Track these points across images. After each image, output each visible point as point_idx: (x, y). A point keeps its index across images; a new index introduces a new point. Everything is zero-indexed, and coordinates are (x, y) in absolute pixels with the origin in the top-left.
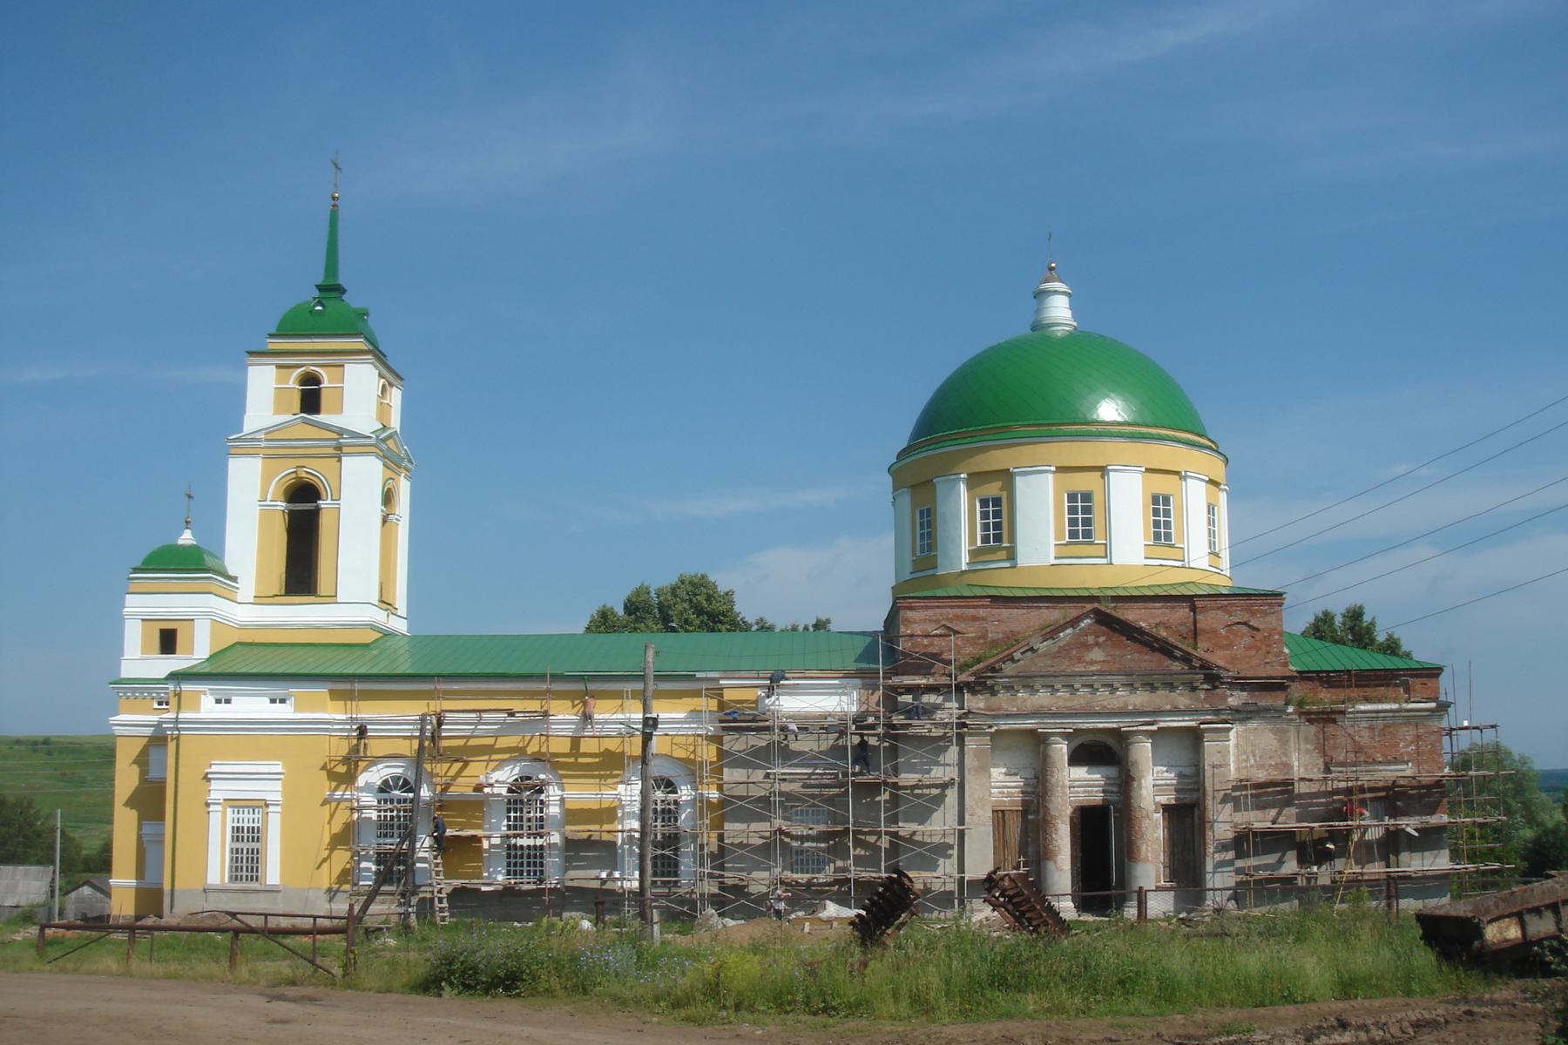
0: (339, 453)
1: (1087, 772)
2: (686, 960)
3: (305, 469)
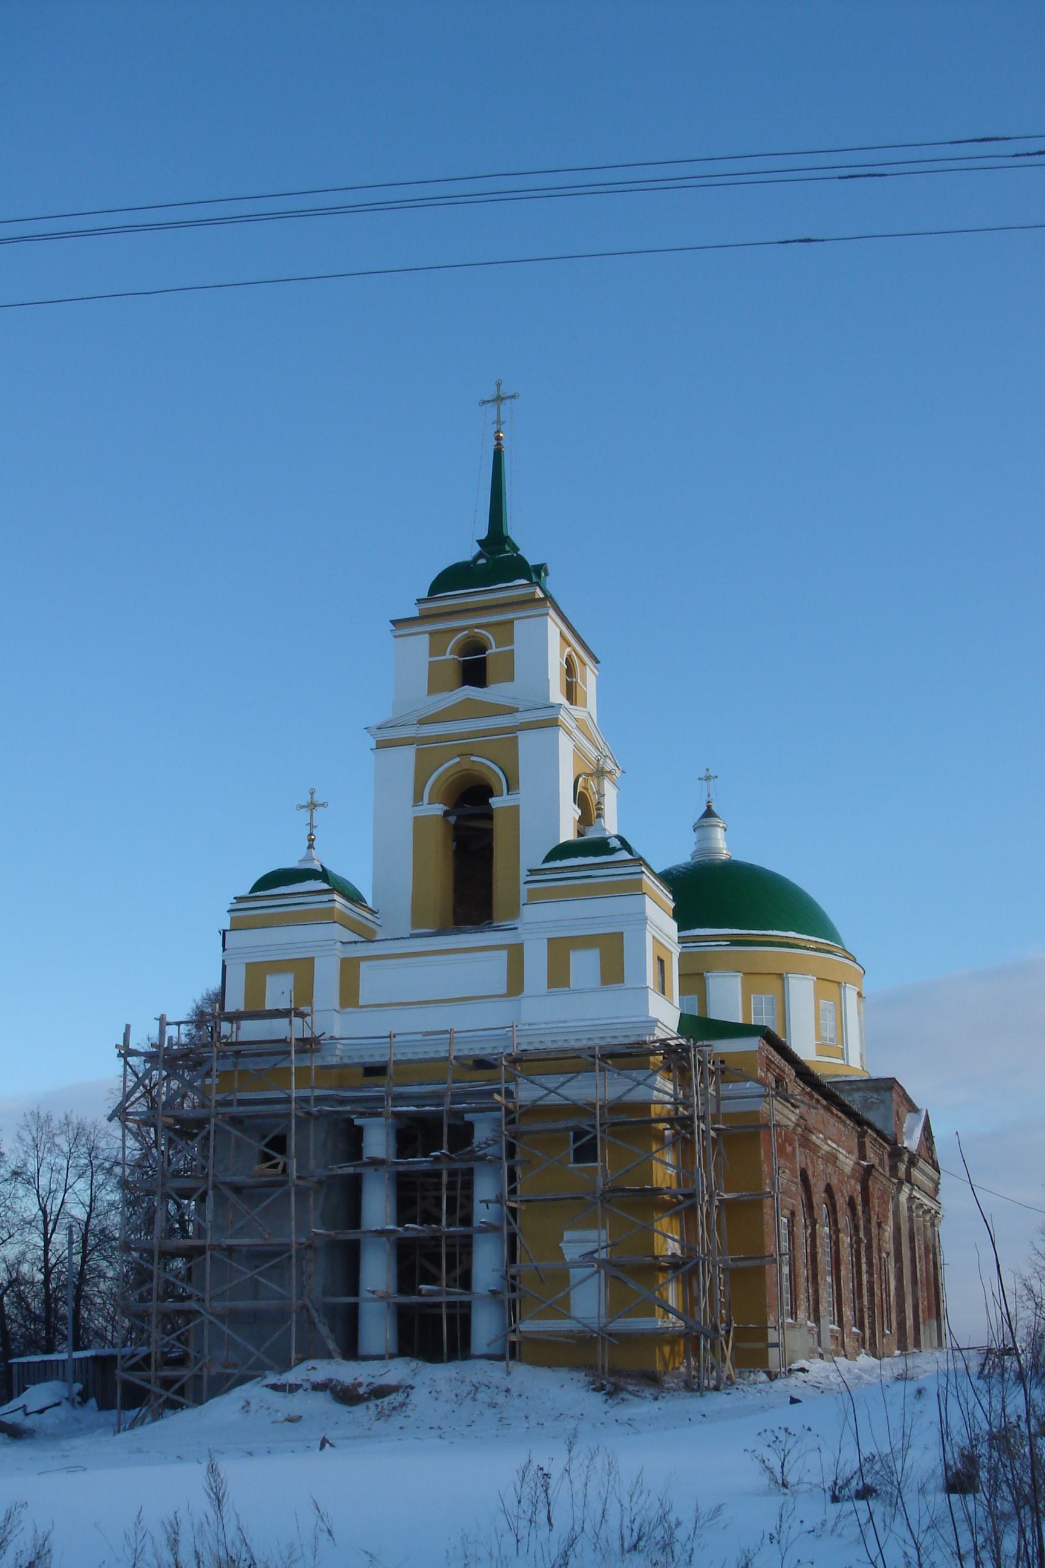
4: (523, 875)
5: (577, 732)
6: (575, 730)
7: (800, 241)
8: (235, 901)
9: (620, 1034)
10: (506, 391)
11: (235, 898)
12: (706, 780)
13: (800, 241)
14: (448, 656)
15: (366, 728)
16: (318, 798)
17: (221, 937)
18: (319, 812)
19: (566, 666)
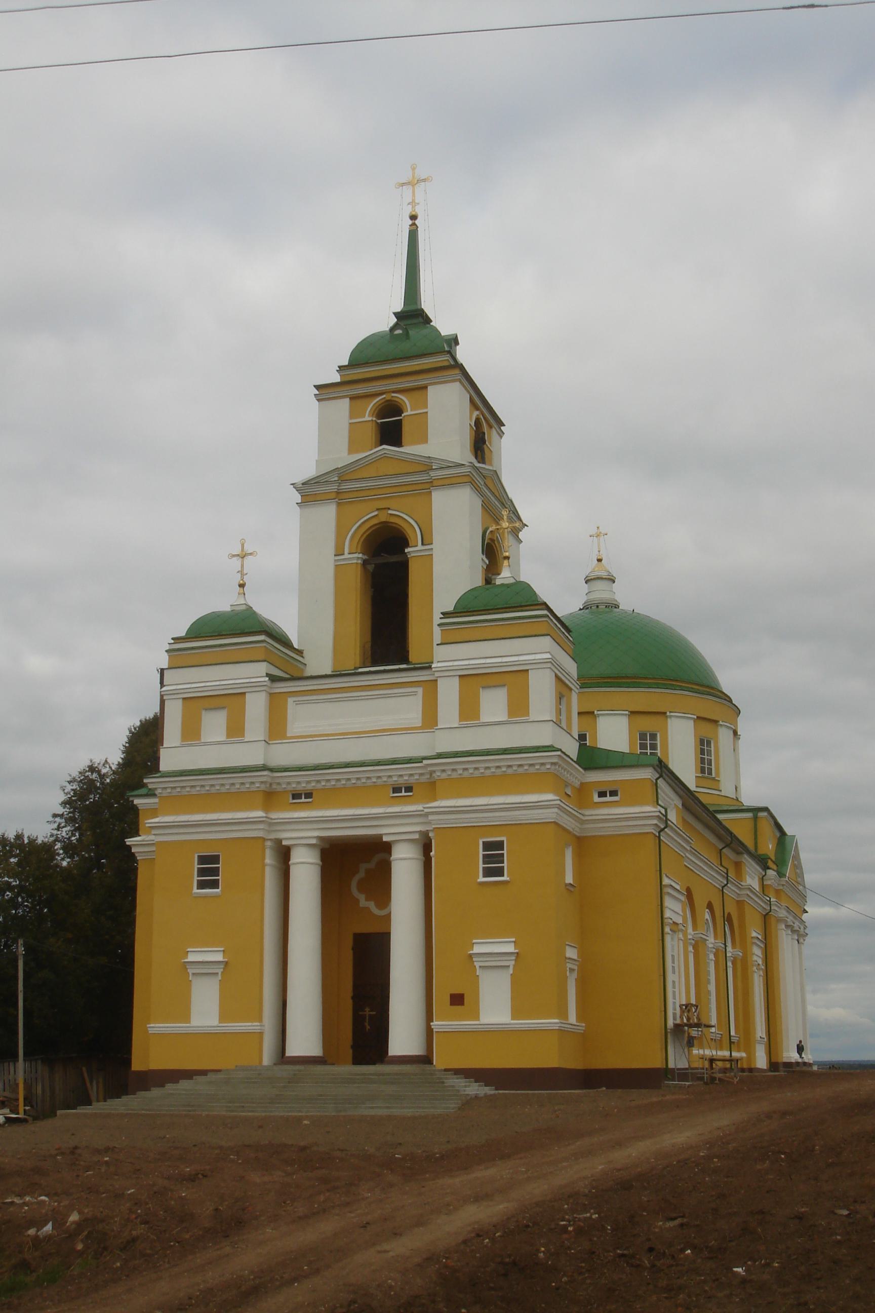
0: (426, 489)
1: (119, 762)
2: (570, 1251)
3: (390, 512)
4: (437, 619)
5: (485, 489)
6: (483, 487)
7: (804, 6)
8: (173, 641)
9: (526, 763)
10: (421, 173)
11: (173, 639)
12: (596, 537)
13: (804, 6)
14: (367, 418)
15: (292, 484)
16: (248, 548)
17: (159, 675)
18: (248, 560)
19: (475, 428)
